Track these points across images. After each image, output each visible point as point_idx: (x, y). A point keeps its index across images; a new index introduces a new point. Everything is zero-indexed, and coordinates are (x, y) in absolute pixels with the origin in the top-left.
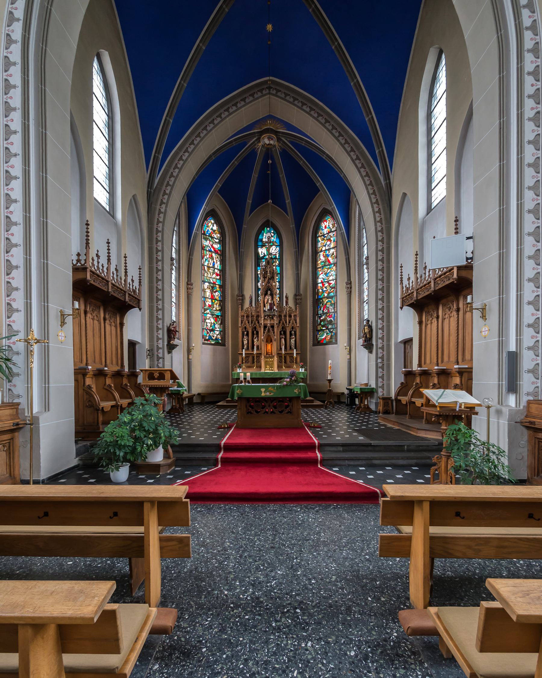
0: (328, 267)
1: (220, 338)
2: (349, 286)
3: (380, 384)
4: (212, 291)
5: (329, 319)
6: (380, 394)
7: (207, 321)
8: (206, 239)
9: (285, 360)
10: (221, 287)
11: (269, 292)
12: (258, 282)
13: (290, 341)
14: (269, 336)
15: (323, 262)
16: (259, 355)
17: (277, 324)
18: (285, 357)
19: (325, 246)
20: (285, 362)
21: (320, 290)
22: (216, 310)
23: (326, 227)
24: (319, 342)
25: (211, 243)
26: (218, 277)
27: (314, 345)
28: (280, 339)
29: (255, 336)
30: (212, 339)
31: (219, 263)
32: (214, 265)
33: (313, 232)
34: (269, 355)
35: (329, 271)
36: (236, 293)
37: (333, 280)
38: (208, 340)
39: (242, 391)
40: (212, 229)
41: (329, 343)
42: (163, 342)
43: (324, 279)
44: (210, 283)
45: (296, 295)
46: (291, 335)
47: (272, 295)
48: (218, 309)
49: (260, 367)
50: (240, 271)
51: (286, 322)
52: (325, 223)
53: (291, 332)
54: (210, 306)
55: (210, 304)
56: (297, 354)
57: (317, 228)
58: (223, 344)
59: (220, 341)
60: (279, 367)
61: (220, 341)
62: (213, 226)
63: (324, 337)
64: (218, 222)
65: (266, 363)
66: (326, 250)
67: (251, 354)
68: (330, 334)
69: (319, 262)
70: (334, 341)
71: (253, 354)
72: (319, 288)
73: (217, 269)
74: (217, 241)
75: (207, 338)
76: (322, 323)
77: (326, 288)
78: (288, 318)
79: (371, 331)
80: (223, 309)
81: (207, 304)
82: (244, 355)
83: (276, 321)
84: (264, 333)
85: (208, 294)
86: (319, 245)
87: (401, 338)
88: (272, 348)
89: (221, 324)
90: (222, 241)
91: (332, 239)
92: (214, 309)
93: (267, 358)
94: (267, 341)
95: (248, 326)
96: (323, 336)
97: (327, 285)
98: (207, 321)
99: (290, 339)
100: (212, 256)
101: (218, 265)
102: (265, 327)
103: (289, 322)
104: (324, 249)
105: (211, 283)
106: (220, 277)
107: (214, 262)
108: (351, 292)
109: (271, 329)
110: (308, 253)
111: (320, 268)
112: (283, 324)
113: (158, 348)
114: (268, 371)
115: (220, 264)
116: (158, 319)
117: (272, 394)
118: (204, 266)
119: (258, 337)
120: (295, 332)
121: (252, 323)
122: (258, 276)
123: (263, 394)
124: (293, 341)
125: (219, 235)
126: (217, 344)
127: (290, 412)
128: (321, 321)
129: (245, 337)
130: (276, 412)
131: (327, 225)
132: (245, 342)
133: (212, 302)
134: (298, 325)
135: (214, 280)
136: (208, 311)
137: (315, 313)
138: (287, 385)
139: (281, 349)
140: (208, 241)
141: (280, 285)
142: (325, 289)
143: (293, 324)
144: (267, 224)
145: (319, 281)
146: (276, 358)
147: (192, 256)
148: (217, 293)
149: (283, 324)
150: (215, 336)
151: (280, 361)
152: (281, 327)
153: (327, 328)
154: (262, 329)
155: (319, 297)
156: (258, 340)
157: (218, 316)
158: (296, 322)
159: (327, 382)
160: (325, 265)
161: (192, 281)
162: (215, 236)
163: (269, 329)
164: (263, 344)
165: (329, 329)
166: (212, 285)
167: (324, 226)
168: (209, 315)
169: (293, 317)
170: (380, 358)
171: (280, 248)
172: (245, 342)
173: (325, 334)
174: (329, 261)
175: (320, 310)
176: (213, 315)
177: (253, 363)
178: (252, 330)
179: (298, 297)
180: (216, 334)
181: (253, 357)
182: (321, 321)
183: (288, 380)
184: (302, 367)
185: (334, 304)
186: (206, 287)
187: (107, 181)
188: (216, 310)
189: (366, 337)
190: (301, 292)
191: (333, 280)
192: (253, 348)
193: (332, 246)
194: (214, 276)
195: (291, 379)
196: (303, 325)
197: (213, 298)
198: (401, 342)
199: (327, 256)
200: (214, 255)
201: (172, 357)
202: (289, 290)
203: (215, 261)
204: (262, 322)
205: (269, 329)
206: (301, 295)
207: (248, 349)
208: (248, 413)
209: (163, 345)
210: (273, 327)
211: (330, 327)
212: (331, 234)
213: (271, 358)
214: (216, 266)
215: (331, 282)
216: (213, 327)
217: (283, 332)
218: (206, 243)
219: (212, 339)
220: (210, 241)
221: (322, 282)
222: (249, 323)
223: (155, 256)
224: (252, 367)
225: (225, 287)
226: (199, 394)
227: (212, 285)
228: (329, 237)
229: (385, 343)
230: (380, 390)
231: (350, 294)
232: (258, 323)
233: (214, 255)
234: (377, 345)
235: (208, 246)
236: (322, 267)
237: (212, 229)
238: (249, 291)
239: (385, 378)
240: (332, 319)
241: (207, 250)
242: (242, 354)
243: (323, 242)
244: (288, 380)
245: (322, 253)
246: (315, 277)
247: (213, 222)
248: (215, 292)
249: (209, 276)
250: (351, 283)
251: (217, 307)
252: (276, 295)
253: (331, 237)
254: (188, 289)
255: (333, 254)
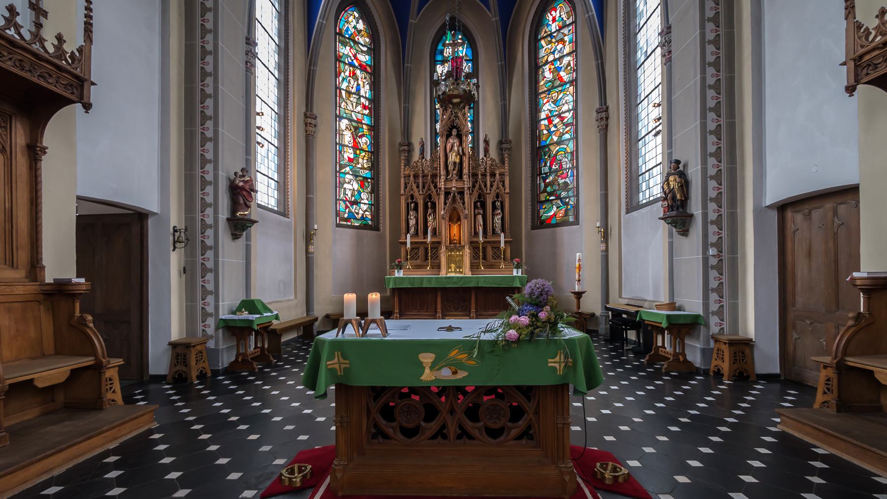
0: (560, 89)
1: (370, 217)
2: (603, 115)
3: (714, 307)
4: (356, 134)
5: (561, 181)
6: (714, 329)
7: (346, 186)
8: (345, 44)
9: (483, 254)
10: (371, 128)
11: (454, 132)
12: (436, 122)
13: (493, 219)
14: (455, 209)
15: (550, 81)
16: (436, 245)
17: (469, 188)
18: (484, 249)
19: (553, 53)
20: (484, 258)
21: (545, 132)
22: (363, 168)
23: (554, 20)
24: (542, 222)
25: (354, 51)
26: (367, 112)
27: (534, 227)
28: (475, 216)
29: (430, 211)
30: (356, 219)
31: (367, 87)
32: (358, 90)
33: (530, 34)
34: (455, 246)
35: (560, 96)
36: (399, 139)
37: (569, 111)
38: (347, 220)
39: (346, 364)
40: (355, 27)
41: (564, 223)
42: (216, 212)
43: (551, 111)
44: (351, 120)
45: (501, 143)
46: (494, 208)
47: (459, 136)
48: (365, 166)
49: (439, 267)
50: (405, 103)
51: (486, 186)
52: (553, 13)
53: (494, 203)
54: (350, 160)
55: (352, 156)
56: (506, 242)
57: (539, 22)
58: (375, 227)
59: (370, 223)
60: (474, 267)
61: (370, 223)
62: (357, 22)
63: (552, 213)
64: (366, 16)
65: (450, 260)
66: (555, 60)
67: (422, 243)
68: (564, 208)
69: (542, 83)
70: (571, 219)
71: (425, 243)
72: (543, 127)
73: (365, 98)
74: (365, 49)
75: (346, 216)
76: (549, 189)
77: (555, 126)
78: (488, 178)
79: (685, 185)
80: (375, 166)
81: (346, 156)
82: (409, 245)
83: (467, 183)
84: (445, 204)
85: (348, 138)
86: (542, 53)
87: (772, 197)
88: (461, 231)
89: (371, 192)
90: (374, 50)
91: (566, 38)
92: (359, 166)
93: (451, 250)
94: (451, 220)
95: (416, 194)
96: (552, 211)
97: (556, 121)
98: (346, 186)
99: (493, 215)
100: (354, 74)
101: (366, 91)
102: (447, 194)
103: (492, 186)
104: (551, 58)
105: (354, 121)
106: (370, 112)
107: (358, 85)
108: (607, 126)
109: (458, 197)
110: (523, 68)
111: (544, 92)
112: (480, 188)
113: (205, 226)
114: (453, 275)
115: (371, 89)
116: (204, 161)
117: (462, 374)
118: (340, 90)
119: (435, 212)
120: (502, 203)
121: (424, 187)
122: (436, 113)
123: (427, 376)
124: (498, 219)
125: (367, 40)
126: (364, 227)
127: (526, 434)
128: (546, 186)
129: (411, 213)
130: (476, 433)
131: (557, 16)
132: (412, 222)
133: (355, 153)
134: (507, 190)
135: (360, 116)
136: (348, 169)
137: (536, 172)
138: (518, 341)
139: (476, 234)
140: (348, 48)
141: (473, 128)
142: (553, 129)
143: (498, 188)
144: (454, 25)
145: (543, 115)
146: (467, 251)
147: (315, 65)
148: (364, 139)
149: (480, 188)
150: (361, 212)
151: (475, 256)
152: (475, 194)
153: (558, 197)
154: (442, 197)
155: (543, 144)
156: (435, 218)
157: (366, 178)
158: (504, 186)
159: (573, 298)
160: (553, 87)
161: (315, 111)
162: (361, 41)
163: (454, 196)
164: (444, 225)
165: (561, 199)
166: (354, 124)
167: (551, 18)
168: (349, 177)
169: (497, 176)
170: (712, 245)
171: (473, 65)
172: (412, 222)
173: (555, 208)
174: (561, 78)
175: (545, 165)
176: (356, 176)
177: (426, 259)
178: (424, 199)
179: (504, 146)
180: (363, 209)
181: (426, 249)
182: (546, 186)
183: (525, 320)
184: (517, 267)
185: (572, 153)
186: (343, 126)
187: (277, 56)
188: (363, 168)
189: (674, 198)
190: (511, 137)
191: (569, 111)
192: (425, 233)
193: (567, 50)
194: (359, 108)
195: (534, 316)
196: (513, 195)
197: (356, 147)
198: (770, 207)
199: (558, 69)
200: (358, 72)
201: (248, 249)
202: (489, 127)
203: (360, 83)
204: (442, 185)
205: (454, 197)
206: (510, 142)
207: (416, 234)
208: (380, 433)
209: (216, 219)
210: (461, 193)
211: (563, 194)
212: (565, 31)
213: (459, 251)
214: (362, 93)
215: (566, 115)
216: (357, 197)
217: (480, 203)
218: (344, 50)
219: (356, 219)
220: (351, 48)
221: (548, 118)
222: (418, 187)
223: (199, 22)
224: (425, 267)
225: (379, 129)
226: (327, 316)
227: (354, 124)
228: (560, 36)
229: (724, 211)
230: (714, 320)
231: (604, 131)
232: (435, 187)
233: (358, 72)
234: (705, 215)
235: (348, 56)
236: (549, 90)
237: (355, 27)
238: (420, 131)
239: (726, 291)
240: (567, 180)
241: (345, 63)
242: (406, 243)
243: (549, 46)
244: (525, 320)
245: (547, 67)
246: (535, 109)
247: (357, 15)
248: (361, 137)
249: (350, 107)
250: (607, 110)
251: (363, 161)
252: (467, 136)
253: (565, 35)
254: (306, 124)
255: (569, 64)
